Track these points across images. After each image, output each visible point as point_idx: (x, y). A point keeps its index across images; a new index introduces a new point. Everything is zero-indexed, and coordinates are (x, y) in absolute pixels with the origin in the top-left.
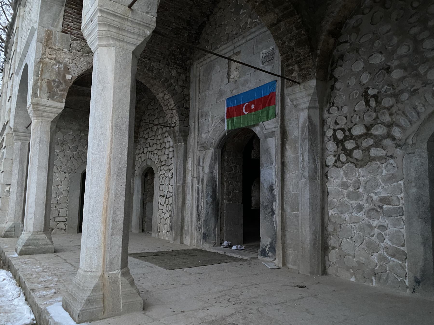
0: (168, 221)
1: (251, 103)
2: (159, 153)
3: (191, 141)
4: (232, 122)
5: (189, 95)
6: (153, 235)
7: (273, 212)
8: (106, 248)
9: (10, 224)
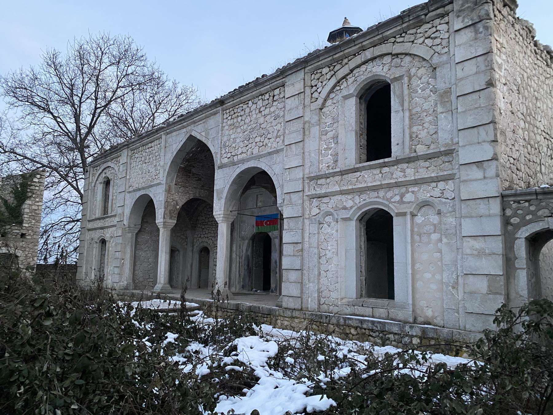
1: (268, 221)
4: (258, 228)
7: (276, 273)
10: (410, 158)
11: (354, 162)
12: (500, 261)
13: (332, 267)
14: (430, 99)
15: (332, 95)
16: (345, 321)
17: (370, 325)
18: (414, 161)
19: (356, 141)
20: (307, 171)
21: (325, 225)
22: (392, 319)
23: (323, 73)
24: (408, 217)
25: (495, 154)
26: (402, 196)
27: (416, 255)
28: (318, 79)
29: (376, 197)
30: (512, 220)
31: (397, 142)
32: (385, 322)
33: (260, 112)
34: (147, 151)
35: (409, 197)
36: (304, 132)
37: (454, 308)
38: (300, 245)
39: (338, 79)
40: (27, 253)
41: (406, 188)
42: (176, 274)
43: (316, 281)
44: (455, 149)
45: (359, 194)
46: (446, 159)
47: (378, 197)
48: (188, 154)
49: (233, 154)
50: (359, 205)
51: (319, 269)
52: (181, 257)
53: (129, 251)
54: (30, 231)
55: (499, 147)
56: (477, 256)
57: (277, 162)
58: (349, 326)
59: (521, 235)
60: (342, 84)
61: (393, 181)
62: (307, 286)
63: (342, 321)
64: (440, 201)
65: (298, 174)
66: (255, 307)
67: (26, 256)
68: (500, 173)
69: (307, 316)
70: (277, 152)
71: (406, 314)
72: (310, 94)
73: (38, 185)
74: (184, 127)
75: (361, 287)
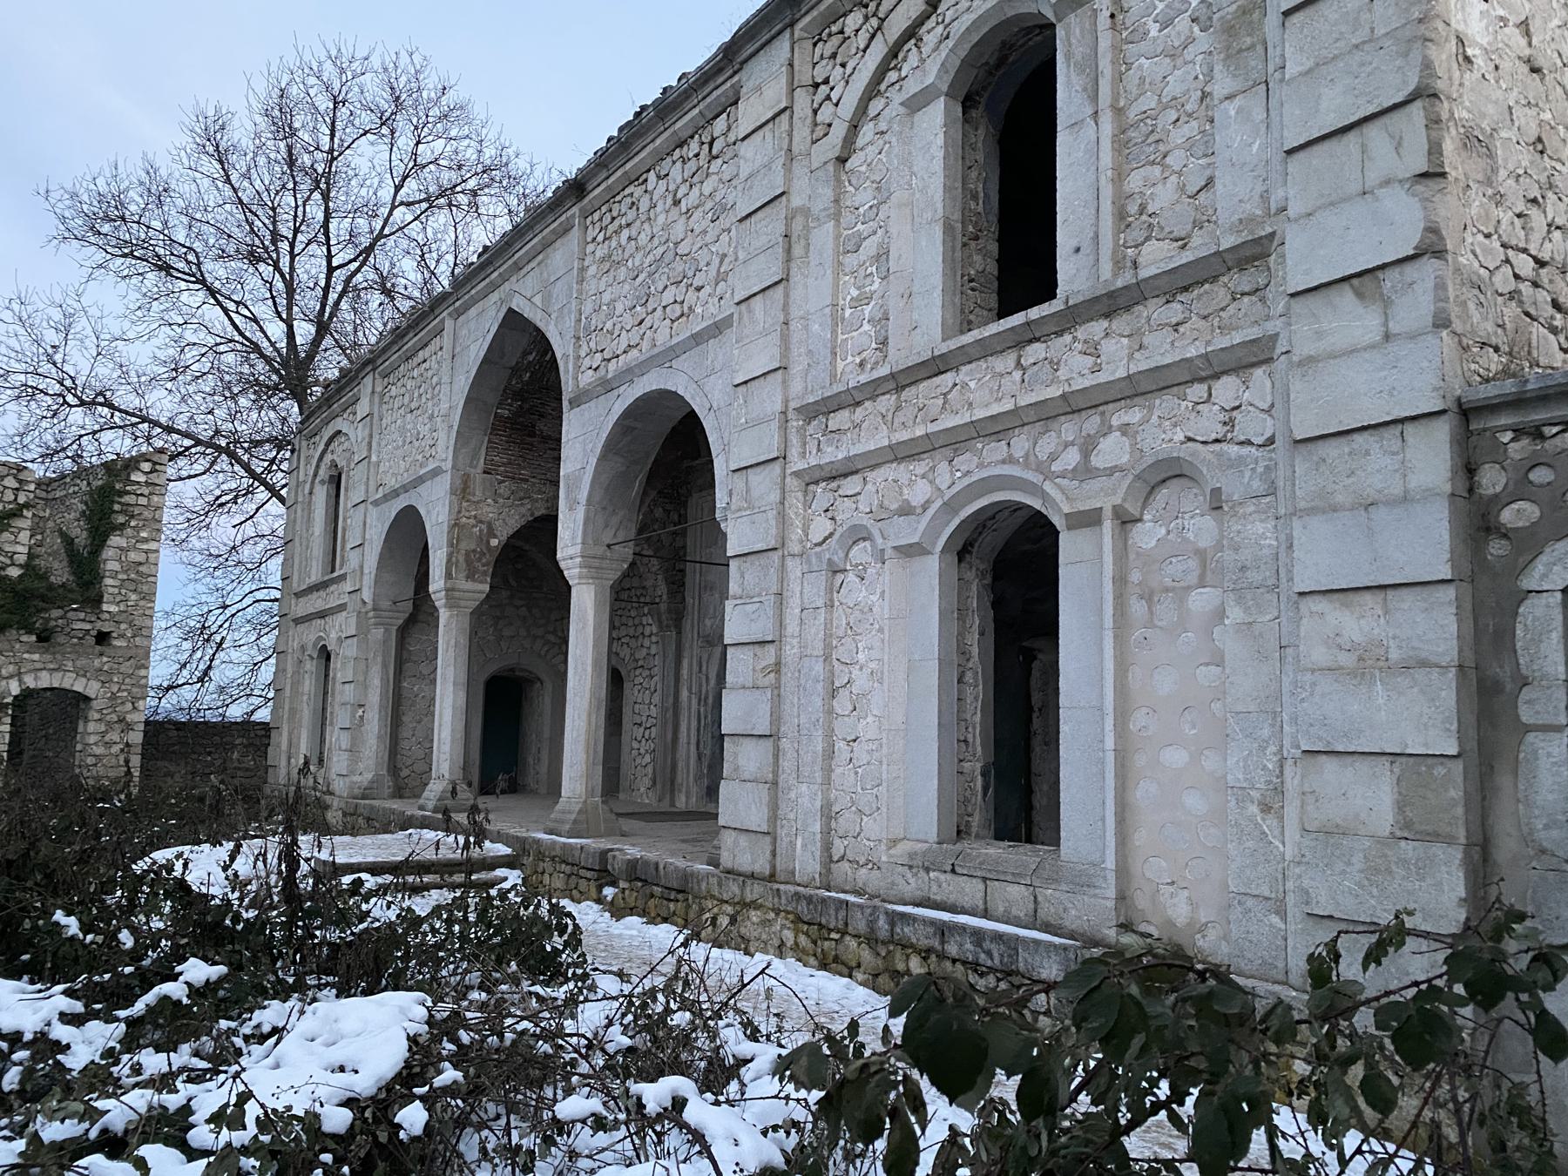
0: (650, 769)
2: (633, 643)
3: (688, 627)
5: (684, 547)
6: (622, 796)
8: (589, 777)
9: (369, 776)
10: (1111, 295)
11: (937, 333)
12: (1446, 692)
13: (867, 727)
14: (1189, 53)
15: (875, 106)
16: (892, 924)
17: (968, 946)
18: (1128, 308)
19: (948, 260)
20: (796, 387)
21: (851, 577)
22: (1047, 928)
23: (848, 31)
24: (1108, 525)
25: (1433, 230)
26: (1088, 447)
27: (1135, 676)
28: (834, 56)
29: (1004, 462)
30: (1507, 516)
31: (1074, 243)
32: (1017, 938)
33: (677, 203)
34: (415, 373)
35: (1112, 451)
36: (789, 251)
37: (1267, 894)
38: (771, 649)
39: (891, 41)
40: (115, 689)
41: (1103, 413)
42: (534, 750)
43: (818, 776)
44: (1273, 234)
45: (948, 452)
46: (1243, 281)
47: (1010, 460)
48: (515, 371)
49: (607, 355)
50: (948, 495)
51: (829, 735)
52: (548, 700)
53: (377, 682)
54: (123, 626)
55: (1451, 200)
56: (1353, 673)
57: (718, 367)
58: (905, 945)
59: (1544, 576)
60: (905, 59)
61: (1054, 392)
62: (793, 795)
63: (882, 922)
64: (1219, 455)
65: (769, 399)
66: (646, 863)
67: (114, 697)
68: (1454, 311)
69: (783, 901)
70: (718, 328)
71: (1092, 911)
72: (810, 112)
73: (146, 492)
74: (494, 287)
75: (965, 802)
